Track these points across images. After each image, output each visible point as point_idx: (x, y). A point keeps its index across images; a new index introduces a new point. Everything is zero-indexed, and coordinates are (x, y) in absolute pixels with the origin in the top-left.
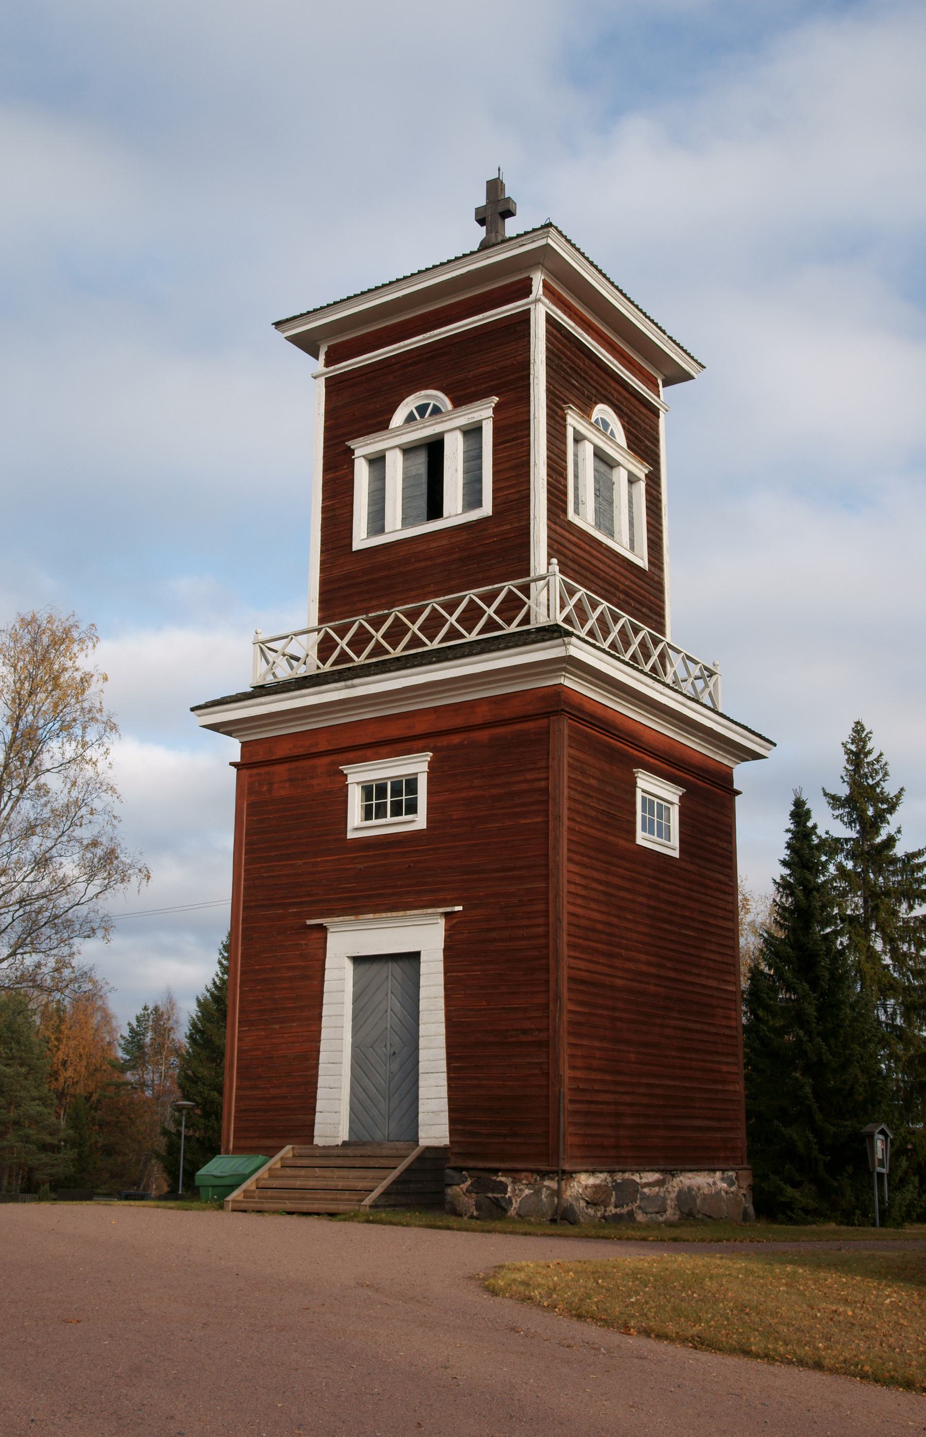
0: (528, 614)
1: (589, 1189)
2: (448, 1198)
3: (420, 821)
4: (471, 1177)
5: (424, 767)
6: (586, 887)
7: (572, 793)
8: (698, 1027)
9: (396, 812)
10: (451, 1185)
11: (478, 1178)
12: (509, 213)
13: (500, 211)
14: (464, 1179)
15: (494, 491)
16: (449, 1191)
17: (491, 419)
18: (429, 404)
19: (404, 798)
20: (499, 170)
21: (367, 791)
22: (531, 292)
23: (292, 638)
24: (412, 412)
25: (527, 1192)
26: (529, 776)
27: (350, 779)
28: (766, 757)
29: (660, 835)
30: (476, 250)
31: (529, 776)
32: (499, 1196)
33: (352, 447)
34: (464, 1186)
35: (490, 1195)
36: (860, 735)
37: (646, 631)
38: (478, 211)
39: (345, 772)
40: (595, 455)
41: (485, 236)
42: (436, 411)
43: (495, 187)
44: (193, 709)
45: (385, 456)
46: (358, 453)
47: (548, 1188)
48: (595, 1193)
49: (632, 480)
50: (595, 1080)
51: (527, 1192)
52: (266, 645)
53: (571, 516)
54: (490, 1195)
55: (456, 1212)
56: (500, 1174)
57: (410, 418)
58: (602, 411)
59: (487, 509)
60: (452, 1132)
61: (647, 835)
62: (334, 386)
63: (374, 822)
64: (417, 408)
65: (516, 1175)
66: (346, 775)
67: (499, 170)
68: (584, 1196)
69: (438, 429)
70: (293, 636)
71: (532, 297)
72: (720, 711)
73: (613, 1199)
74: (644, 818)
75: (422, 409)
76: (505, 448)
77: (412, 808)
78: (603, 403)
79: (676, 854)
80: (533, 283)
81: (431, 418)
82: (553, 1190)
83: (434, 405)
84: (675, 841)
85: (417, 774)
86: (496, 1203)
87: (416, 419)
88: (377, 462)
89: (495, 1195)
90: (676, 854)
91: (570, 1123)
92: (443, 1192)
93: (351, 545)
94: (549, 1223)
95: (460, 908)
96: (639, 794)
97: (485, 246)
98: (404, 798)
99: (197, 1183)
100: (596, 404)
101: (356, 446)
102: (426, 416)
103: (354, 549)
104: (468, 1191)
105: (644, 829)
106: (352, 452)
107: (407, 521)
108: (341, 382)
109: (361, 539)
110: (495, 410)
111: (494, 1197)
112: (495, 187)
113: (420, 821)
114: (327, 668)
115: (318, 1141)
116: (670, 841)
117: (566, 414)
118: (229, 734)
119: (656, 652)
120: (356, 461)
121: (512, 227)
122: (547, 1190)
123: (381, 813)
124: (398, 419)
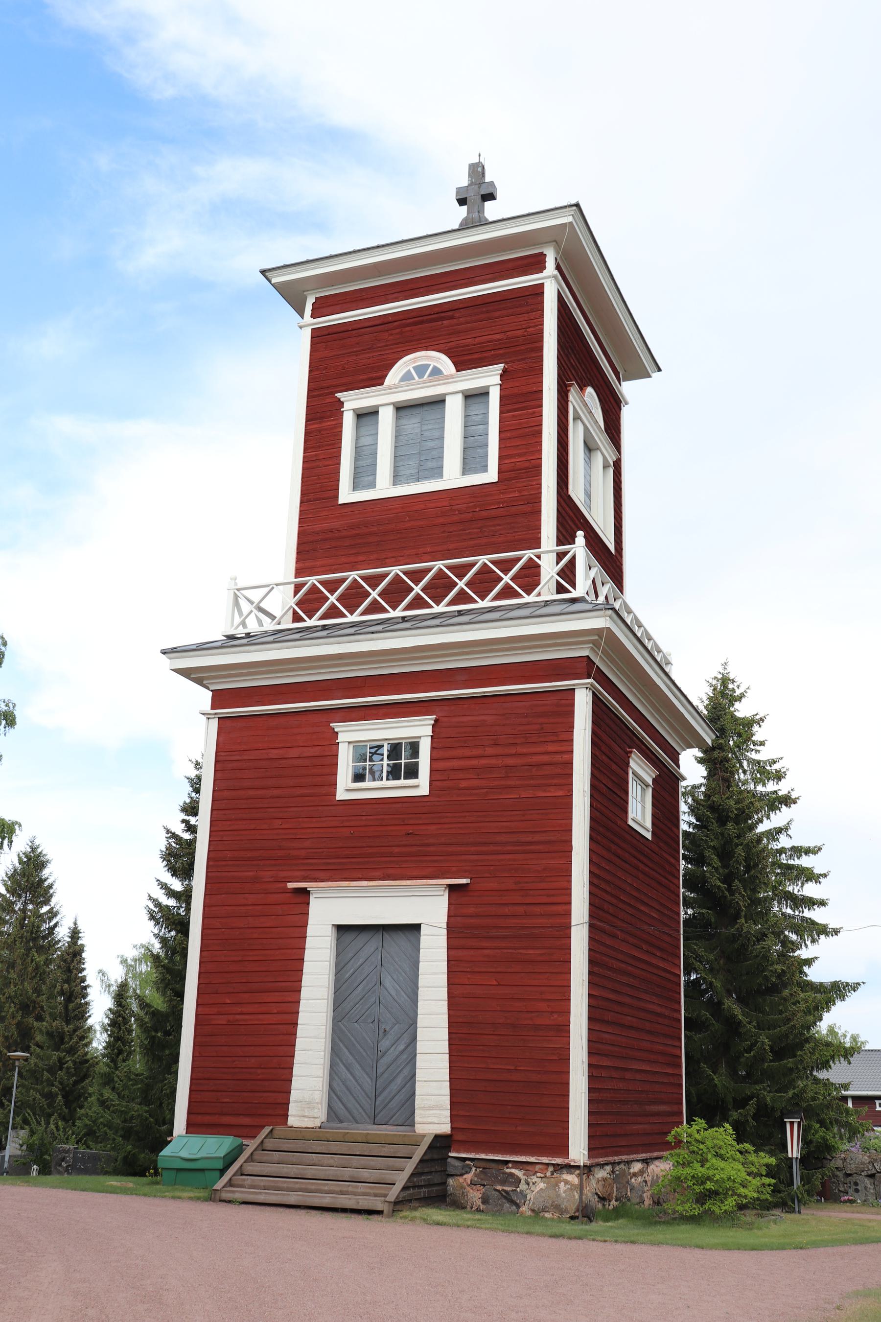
2: (450, 1190)
3: (421, 786)
4: (477, 1167)
9: (394, 773)
10: (452, 1175)
11: (484, 1168)
12: (490, 196)
13: (483, 193)
14: (468, 1170)
15: (500, 458)
16: (451, 1181)
17: (499, 387)
18: (429, 365)
19: (403, 761)
20: (480, 155)
22: (545, 268)
23: (273, 588)
25: (542, 1185)
26: (551, 748)
27: (341, 738)
30: (457, 227)
31: (551, 748)
33: (341, 400)
34: (469, 1177)
38: (459, 190)
39: (336, 730)
41: (466, 215)
42: (436, 372)
43: (477, 171)
44: (164, 652)
45: (378, 411)
47: (566, 1182)
51: (542, 1185)
52: (241, 591)
54: (499, 1188)
55: (458, 1205)
56: (510, 1165)
57: (407, 377)
60: (454, 1118)
62: (318, 336)
65: (530, 1167)
67: (480, 155)
68: (597, 1191)
70: (275, 586)
71: (546, 273)
76: (513, 416)
77: (412, 772)
80: (547, 259)
82: (572, 1185)
83: (414, 368)
85: (420, 737)
86: (507, 1197)
88: (367, 416)
89: (506, 1188)
91: (10, 848)
92: (444, 1183)
93: (337, 497)
94: (568, 1219)
97: (466, 226)
98: (403, 761)
99: (160, 1165)
103: (341, 501)
104: (472, 1183)
106: (342, 404)
108: (329, 334)
109: (346, 495)
111: (503, 1190)
112: (477, 171)
113: (421, 786)
117: (568, 391)
118: (199, 681)
120: (345, 413)
121: (491, 210)
122: (565, 1185)
124: (394, 376)
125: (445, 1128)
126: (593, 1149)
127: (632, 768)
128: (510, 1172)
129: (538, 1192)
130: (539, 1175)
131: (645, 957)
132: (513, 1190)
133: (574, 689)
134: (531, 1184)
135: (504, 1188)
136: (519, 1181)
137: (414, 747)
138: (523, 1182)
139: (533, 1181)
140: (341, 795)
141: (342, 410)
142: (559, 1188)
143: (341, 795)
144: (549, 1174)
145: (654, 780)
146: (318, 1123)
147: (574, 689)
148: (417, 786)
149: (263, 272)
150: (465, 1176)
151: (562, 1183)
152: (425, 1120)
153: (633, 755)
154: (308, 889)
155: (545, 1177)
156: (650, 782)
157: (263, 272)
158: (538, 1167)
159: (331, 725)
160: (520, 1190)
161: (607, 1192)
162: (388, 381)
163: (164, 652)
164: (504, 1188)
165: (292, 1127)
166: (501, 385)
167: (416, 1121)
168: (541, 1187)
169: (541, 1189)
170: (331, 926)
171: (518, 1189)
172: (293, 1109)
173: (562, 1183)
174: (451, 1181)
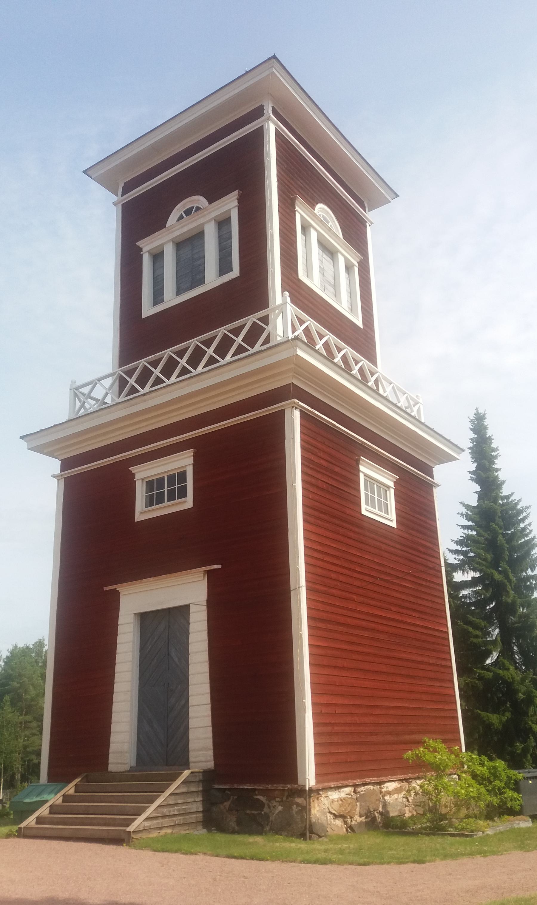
0: (268, 336)
1: (335, 803)
3: (188, 502)
5: (191, 461)
6: (321, 544)
7: (305, 469)
8: (419, 659)
9: (171, 497)
21: (150, 485)
24: (182, 215)
25: (280, 808)
28: (458, 459)
29: (380, 509)
32: (255, 812)
35: (248, 812)
36: (513, 493)
37: (364, 362)
40: (319, 242)
44: (22, 438)
46: (144, 250)
48: (341, 806)
49: (349, 268)
50: (336, 705)
51: (280, 808)
53: (302, 275)
54: (248, 812)
58: (321, 208)
59: (235, 272)
61: (369, 508)
63: (155, 507)
64: (184, 212)
66: (134, 474)
68: (331, 810)
69: (201, 221)
72: (423, 421)
73: (358, 809)
74: (366, 495)
75: (188, 212)
77: (183, 493)
78: (322, 203)
79: (394, 524)
81: (196, 214)
84: (393, 515)
85: (185, 466)
87: (184, 218)
90: (394, 524)
95: (220, 566)
96: (362, 476)
100: (317, 203)
101: (144, 245)
102: (192, 213)
105: (367, 503)
106: (141, 250)
107: (179, 291)
110: (239, 201)
111: (252, 814)
114: (122, 399)
115: (111, 768)
116: (388, 514)
119: (373, 379)
123: (160, 500)
125: (211, 765)
126: (319, 775)
127: (363, 472)
128: (257, 798)
129: (277, 814)
130: (277, 799)
131: (398, 617)
132: (259, 814)
133: (284, 409)
134: (272, 808)
135: (252, 812)
136: (262, 805)
137: (182, 476)
138: (266, 806)
139: (273, 805)
140: (139, 517)
141: (141, 253)
142: (292, 810)
143: (139, 517)
144: (285, 798)
145: (395, 482)
146: (127, 768)
147: (284, 409)
148: (185, 502)
149: (85, 172)
150: (225, 804)
151: (295, 806)
152: (197, 759)
153: (361, 462)
154: (117, 590)
155: (282, 801)
156: (391, 484)
157: (85, 172)
158: (276, 792)
159: (129, 469)
160: (264, 813)
161: (345, 810)
162: (168, 224)
163: (22, 438)
164: (252, 812)
165: (111, 772)
166: (238, 206)
167: (190, 761)
168: (279, 810)
169: (280, 811)
170: (133, 616)
171: (263, 812)
172: (112, 758)
173: (295, 806)
174: (214, 809)
